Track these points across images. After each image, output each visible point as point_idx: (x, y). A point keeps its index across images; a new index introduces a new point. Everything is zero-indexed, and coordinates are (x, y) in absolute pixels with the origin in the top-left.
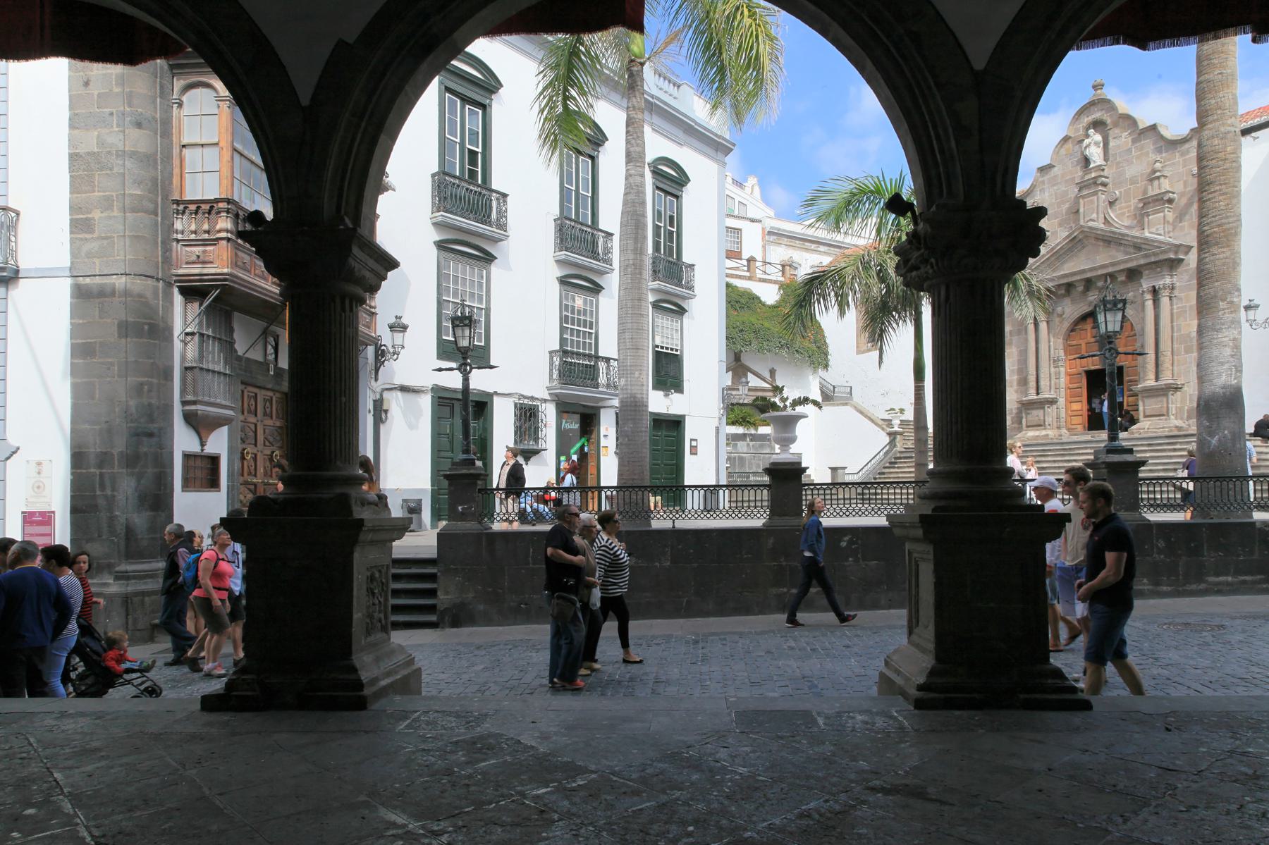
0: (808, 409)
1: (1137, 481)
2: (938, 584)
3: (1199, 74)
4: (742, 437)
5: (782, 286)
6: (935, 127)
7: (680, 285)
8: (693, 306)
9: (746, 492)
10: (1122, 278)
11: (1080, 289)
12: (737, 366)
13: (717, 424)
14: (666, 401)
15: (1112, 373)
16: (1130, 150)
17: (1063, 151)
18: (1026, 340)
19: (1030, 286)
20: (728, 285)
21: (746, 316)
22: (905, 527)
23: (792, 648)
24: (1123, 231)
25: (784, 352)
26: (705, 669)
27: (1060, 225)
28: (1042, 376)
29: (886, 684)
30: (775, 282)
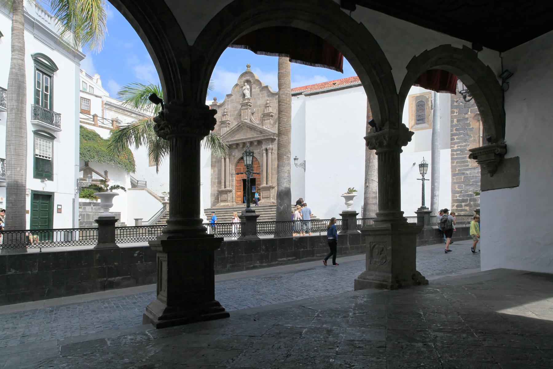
0: (119, 191)
1: (256, 224)
2: (169, 272)
3: (279, 69)
4: (90, 204)
5: (111, 131)
6: (172, 67)
7: (52, 124)
8: (60, 136)
9: (141, 229)
10: (256, 144)
11: (241, 146)
12: (86, 168)
13: (73, 197)
14: (43, 185)
15: (248, 181)
16: (259, 94)
17: (236, 90)
18: (221, 165)
19: (220, 143)
20: (81, 127)
21: (91, 144)
22: (156, 246)
23: (106, 308)
24: (256, 125)
25: (112, 163)
26: (54, 325)
27: (234, 119)
28: (227, 180)
29: (147, 320)
30: (108, 128)
